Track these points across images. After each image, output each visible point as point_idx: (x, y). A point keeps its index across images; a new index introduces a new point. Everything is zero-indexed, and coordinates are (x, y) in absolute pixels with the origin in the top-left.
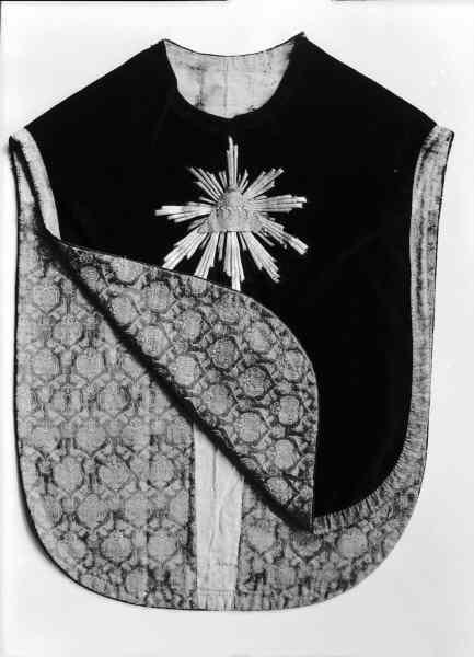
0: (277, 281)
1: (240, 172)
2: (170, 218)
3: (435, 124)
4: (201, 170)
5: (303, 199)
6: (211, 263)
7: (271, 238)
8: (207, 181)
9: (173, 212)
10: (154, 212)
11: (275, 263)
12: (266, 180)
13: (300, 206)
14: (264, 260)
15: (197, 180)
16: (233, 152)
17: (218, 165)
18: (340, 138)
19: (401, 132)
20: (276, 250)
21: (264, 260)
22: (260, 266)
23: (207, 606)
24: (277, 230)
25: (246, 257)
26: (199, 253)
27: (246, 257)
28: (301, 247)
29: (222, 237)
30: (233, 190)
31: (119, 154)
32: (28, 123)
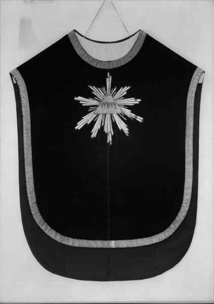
0: (127, 135)
1: (112, 87)
2: (81, 102)
3: (196, 67)
4: (94, 87)
5: (139, 100)
6: (99, 127)
7: (126, 116)
8: (95, 90)
9: (80, 125)
10: (74, 98)
11: (127, 127)
12: (124, 90)
13: (138, 103)
14: (122, 126)
15: (93, 91)
16: (109, 81)
17: (101, 84)
18: (159, 75)
19: (186, 69)
20: (128, 121)
21: (122, 126)
22: (120, 129)
23: (81, 49)
24: (128, 113)
25: (114, 125)
26: (93, 123)
27: (114, 125)
28: (140, 119)
29: (104, 116)
30: (108, 95)
31: (55, 77)
32: (150, 35)
